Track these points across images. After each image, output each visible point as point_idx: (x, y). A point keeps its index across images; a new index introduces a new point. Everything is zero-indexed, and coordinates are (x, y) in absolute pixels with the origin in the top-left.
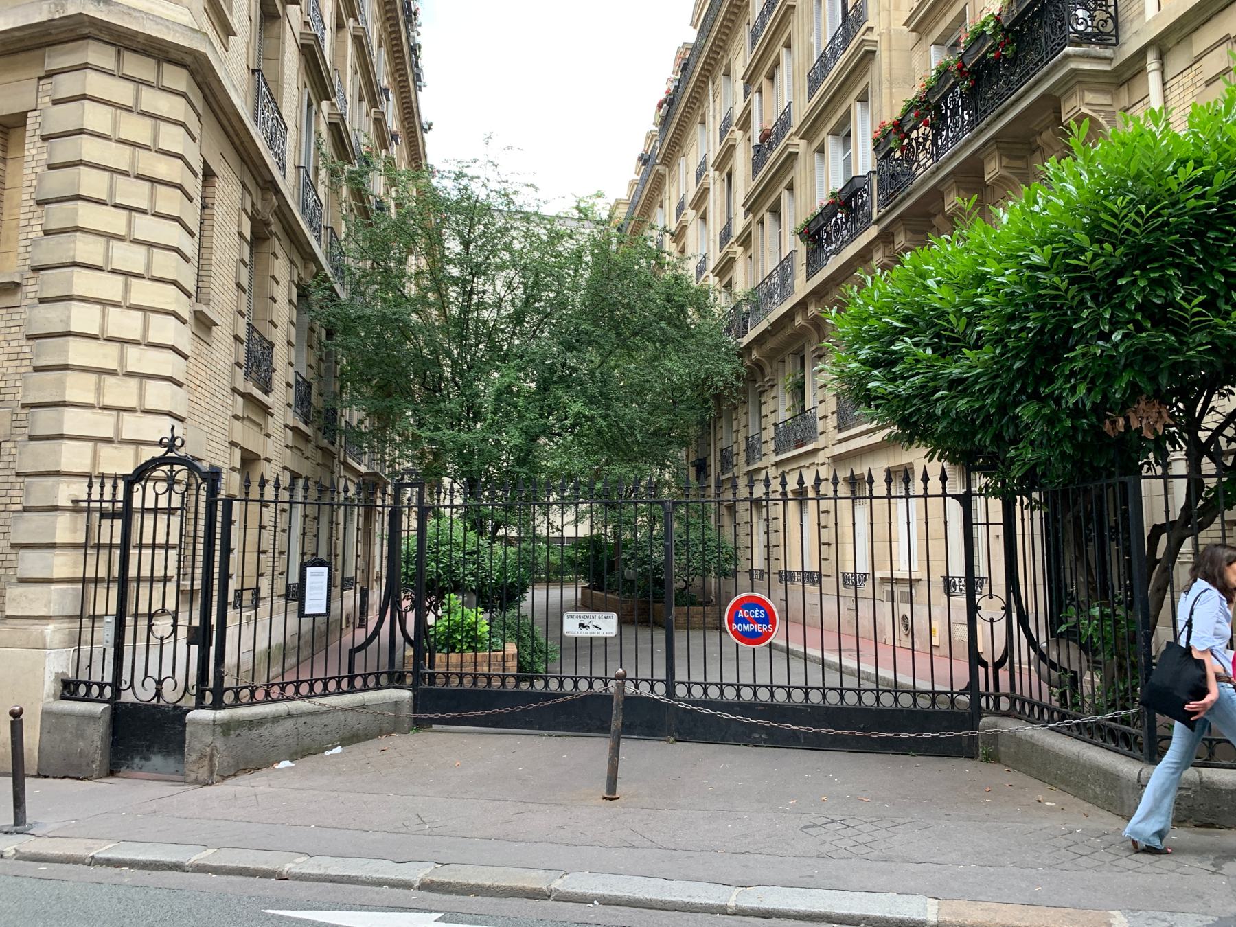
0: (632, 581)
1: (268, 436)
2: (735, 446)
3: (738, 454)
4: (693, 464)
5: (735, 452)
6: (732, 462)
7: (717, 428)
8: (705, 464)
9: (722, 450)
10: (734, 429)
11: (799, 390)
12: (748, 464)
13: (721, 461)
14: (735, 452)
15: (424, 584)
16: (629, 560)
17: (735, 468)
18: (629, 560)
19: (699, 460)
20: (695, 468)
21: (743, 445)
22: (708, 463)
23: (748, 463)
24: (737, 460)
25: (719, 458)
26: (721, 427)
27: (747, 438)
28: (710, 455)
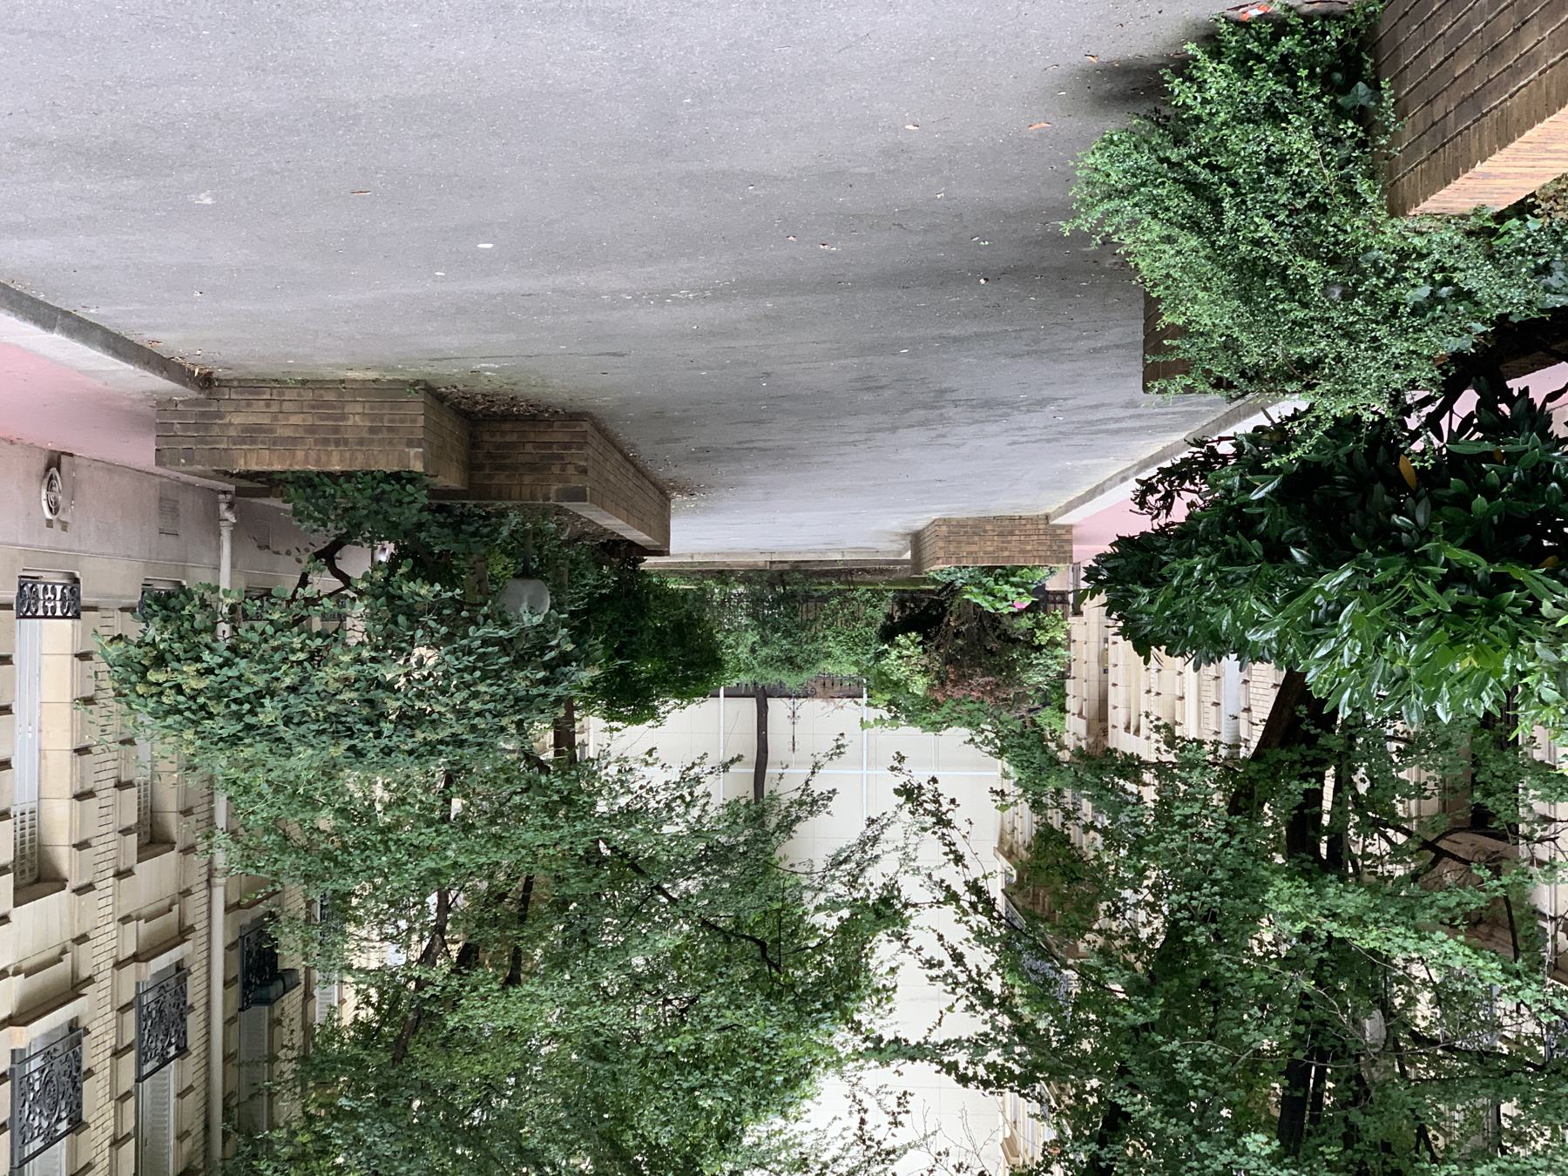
0: (525, 574)
1: (839, 749)
2: (127, 1081)
3: (117, 1053)
4: (286, 979)
5: (130, 1057)
6: (141, 1019)
7: (197, 1129)
8: (246, 985)
9: (182, 1051)
10: (129, 1148)
11: (1013, 615)
12: (180, 968)
13: (183, 1009)
14: (130, 1057)
15: (160, 470)
16: (565, 659)
17: (128, 995)
18: (565, 659)
19: (269, 1002)
20: (285, 964)
21: (95, 1096)
22: (236, 989)
23: (75, 1030)
24: (120, 1028)
25: (194, 1023)
26: (181, 1137)
27: (77, 1124)
28: (228, 1023)
